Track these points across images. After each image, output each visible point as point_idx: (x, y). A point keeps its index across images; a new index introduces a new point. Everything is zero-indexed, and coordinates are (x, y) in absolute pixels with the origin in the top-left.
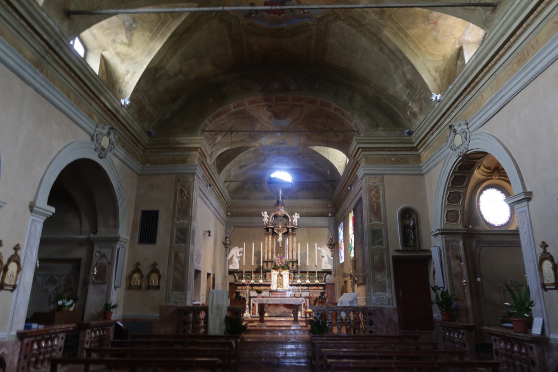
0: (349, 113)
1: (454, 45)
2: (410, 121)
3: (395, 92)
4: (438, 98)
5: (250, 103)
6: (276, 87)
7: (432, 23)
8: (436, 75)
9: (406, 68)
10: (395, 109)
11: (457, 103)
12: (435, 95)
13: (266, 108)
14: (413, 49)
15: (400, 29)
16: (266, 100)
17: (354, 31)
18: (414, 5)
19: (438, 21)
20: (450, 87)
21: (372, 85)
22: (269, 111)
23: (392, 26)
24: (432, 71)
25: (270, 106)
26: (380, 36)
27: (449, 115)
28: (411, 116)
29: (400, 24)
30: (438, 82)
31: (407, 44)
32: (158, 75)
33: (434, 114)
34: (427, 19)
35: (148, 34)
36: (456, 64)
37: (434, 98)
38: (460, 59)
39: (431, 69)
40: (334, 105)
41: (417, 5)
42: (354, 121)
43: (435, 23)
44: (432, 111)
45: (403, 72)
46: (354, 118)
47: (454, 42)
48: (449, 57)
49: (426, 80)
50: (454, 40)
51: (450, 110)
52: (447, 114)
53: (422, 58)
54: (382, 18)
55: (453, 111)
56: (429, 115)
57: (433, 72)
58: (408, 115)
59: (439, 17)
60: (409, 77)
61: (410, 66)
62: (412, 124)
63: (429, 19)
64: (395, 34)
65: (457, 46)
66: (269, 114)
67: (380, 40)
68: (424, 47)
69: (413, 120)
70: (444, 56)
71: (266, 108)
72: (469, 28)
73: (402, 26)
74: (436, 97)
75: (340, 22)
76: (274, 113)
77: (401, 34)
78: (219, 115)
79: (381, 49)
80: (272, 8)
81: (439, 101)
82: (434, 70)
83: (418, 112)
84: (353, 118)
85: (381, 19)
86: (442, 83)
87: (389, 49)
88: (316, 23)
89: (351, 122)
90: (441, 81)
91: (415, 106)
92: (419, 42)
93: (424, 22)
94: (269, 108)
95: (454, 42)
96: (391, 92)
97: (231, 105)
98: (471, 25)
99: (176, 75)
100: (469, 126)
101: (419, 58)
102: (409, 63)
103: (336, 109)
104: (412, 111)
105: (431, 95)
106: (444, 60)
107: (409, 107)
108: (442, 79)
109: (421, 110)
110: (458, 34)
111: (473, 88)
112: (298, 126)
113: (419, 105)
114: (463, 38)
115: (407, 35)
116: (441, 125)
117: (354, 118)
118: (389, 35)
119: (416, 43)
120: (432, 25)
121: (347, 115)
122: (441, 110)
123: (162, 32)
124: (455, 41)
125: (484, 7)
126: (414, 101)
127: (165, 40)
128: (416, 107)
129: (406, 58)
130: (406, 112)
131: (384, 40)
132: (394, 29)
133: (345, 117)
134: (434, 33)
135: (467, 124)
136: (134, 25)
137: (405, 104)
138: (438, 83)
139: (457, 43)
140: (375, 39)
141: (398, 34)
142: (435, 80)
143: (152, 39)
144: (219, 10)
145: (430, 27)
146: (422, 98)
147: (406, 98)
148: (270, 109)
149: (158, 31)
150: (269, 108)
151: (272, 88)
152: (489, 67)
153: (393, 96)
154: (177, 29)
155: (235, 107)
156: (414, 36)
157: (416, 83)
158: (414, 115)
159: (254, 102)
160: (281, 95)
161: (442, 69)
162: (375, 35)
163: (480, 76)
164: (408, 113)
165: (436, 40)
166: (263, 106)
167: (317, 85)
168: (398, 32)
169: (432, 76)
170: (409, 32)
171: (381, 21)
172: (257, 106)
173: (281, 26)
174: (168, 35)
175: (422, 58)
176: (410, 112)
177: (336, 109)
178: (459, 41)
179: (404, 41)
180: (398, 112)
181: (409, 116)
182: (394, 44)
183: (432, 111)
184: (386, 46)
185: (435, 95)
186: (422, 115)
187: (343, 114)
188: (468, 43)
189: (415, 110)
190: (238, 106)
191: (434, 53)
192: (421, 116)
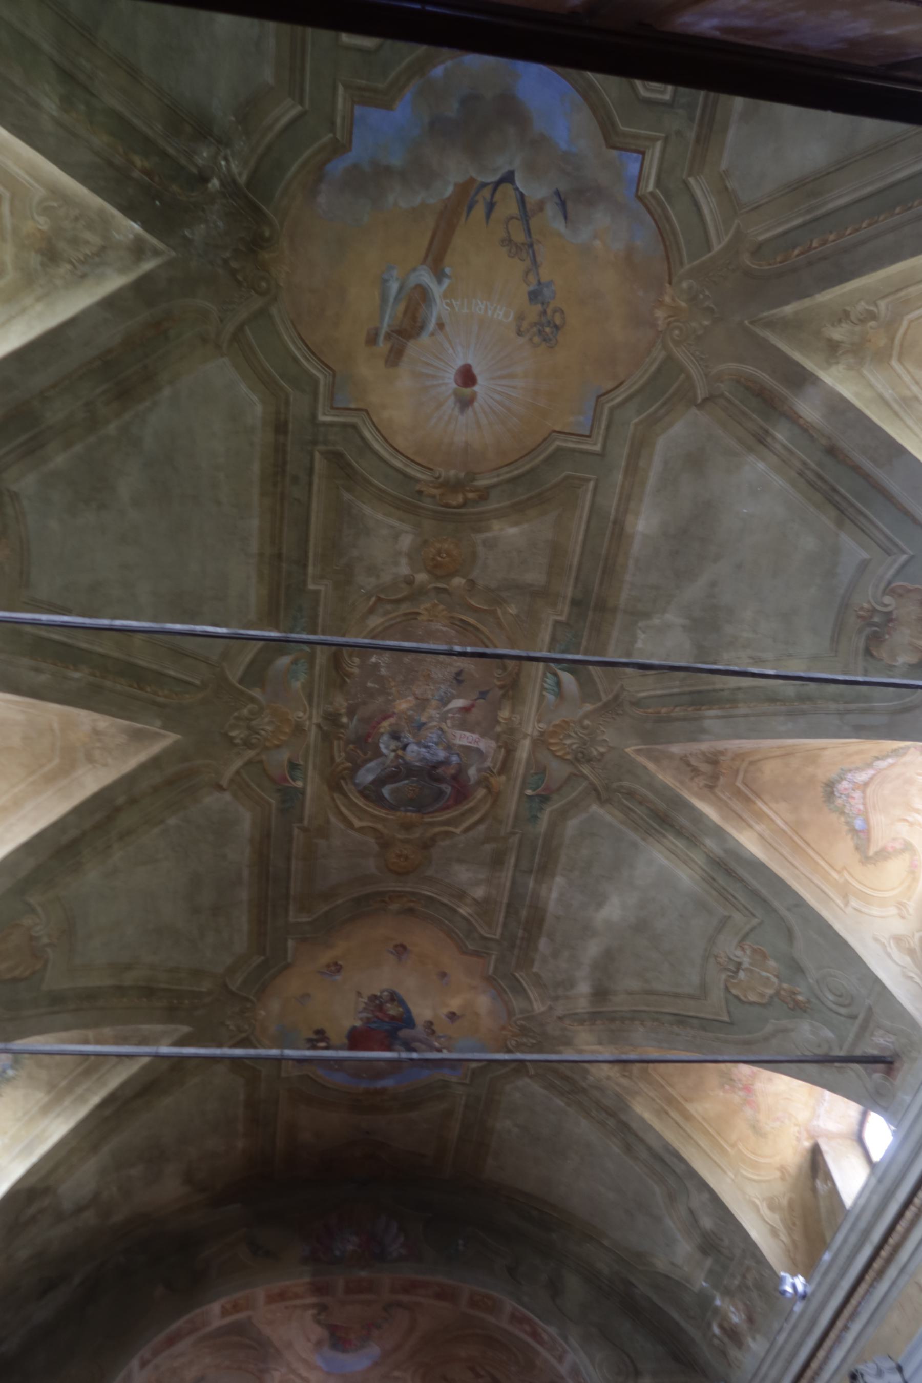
0: (552, 1330)
1: (798, 1139)
2: (724, 1354)
3: (673, 1264)
4: (800, 1288)
5: (271, 1299)
6: (350, 1247)
7: (740, 1089)
8: (774, 1218)
9: (697, 1200)
10: (675, 1316)
11: (854, 1302)
12: (789, 1279)
13: (311, 1312)
14: (708, 1151)
15: (671, 1100)
16: (319, 1289)
17: (560, 1102)
18: (720, 1058)
19: (752, 1085)
20: (827, 1257)
21: (606, 1242)
22: (318, 1322)
23: (652, 1094)
24: (760, 1207)
25: (323, 1308)
26: (624, 1118)
27: (839, 1339)
28: (726, 1340)
29: (669, 1089)
30: (784, 1237)
31: (691, 1137)
32: (32, 1211)
33: (796, 1336)
34: (730, 1080)
35: (41, 1097)
36: (814, 1190)
37: (789, 1289)
38: (821, 1174)
39: (757, 1202)
40: (510, 1305)
41: (726, 1058)
42: (570, 1358)
43: (748, 1089)
44: (788, 1327)
45: (691, 1212)
46: (567, 1348)
47: (797, 1134)
48: (792, 1170)
49: (754, 1234)
50: (796, 1129)
51: (840, 1324)
52: (833, 1335)
53: (731, 1174)
54: (626, 1074)
55: (846, 1328)
56: (781, 1339)
57: (765, 1210)
58: (714, 1335)
59: (754, 1076)
60: (707, 1223)
61: (706, 1196)
62: (730, 1365)
63: (732, 1080)
64: (661, 1113)
65: (807, 1144)
66: (318, 1332)
67: (624, 1127)
68: (733, 1146)
69: (733, 1352)
70: (782, 1169)
71: (311, 1312)
72: (824, 1100)
73: (674, 1093)
74: (794, 1286)
75: (527, 1080)
76: (333, 1329)
77: (674, 1114)
78: (171, 1341)
79: (628, 1149)
80: (399, 1055)
81: (804, 1297)
82: (765, 1204)
83: (744, 1326)
84: (564, 1344)
85: (624, 1076)
86: (794, 1242)
87: (649, 1149)
88: (467, 1081)
89: (560, 1359)
90: (789, 1235)
91: (732, 1309)
92: (719, 1134)
93: (722, 1086)
94: (319, 1314)
95: (797, 1134)
96: (661, 1264)
97: (215, 1307)
98: (827, 1094)
99: (80, 1210)
100: (907, 1373)
101: (725, 1172)
102: (704, 1186)
103: (515, 1318)
104: (726, 1325)
105: (781, 1280)
106: (783, 1178)
107: (716, 1311)
108: (790, 1231)
109: (750, 1320)
110: (802, 1115)
111: (889, 1261)
112: (397, 1374)
113: (745, 1304)
114: (815, 1123)
115: (688, 1117)
116: (820, 1368)
117: (567, 1348)
118: (647, 1115)
119: (711, 1134)
120: (741, 1093)
121: (546, 1337)
122: (813, 1323)
123: (79, 1091)
124: (799, 1132)
125: (865, 1065)
126: (727, 1292)
127: (82, 1112)
128: (737, 1309)
129: (693, 1174)
130: (709, 1326)
131: (634, 1125)
132: (658, 1101)
133: (541, 1342)
134: (748, 1112)
135: (900, 1369)
136: (10, 1072)
137: (704, 1302)
138: (783, 1242)
139: (805, 1134)
140: (611, 1122)
141: (667, 1113)
142: (774, 1232)
143: (46, 1110)
144: (270, 1055)
145: (737, 1098)
146: (750, 1283)
147: (704, 1284)
148: (322, 1317)
149: (69, 1089)
150: (319, 1314)
151: (337, 1253)
152: (916, 1207)
153: (668, 1277)
154: (123, 1086)
155: (225, 1312)
156: (704, 1119)
157: (726, 1242)
158: (733, 1335)
159: (282, 1296)
160: (363, 1274)
161: (784, 1202)
162: (612, 1114)
163: (900, 1228)
164: (716, 1330)
165: (756, 1129)
166: (306, 1307)
167: (461, 1242)
168: (666, 1108)
169: (768, 1223)
170: (691, 1108)
171: (624, 1081)
172: (287, 1307)
173: (380, 1084)
174: (95, 1100)
175: (731, 1174)
176: (721, 1327)
177: (515, 1318)
178: (808, 1131)
179: (684, 1130)
180: (683, 1323)
181: (719, 1339)
182: (659, 1137)
183: (788, 1327)
184: (642, 1141)
185: (789, 1279)
186: (758, 1337)
187: (535, 1335)
188: (830, 1136)
189: (735, 1319)
190: (236, 1307)
191: (756, 1161)
192: (754, 1339)
